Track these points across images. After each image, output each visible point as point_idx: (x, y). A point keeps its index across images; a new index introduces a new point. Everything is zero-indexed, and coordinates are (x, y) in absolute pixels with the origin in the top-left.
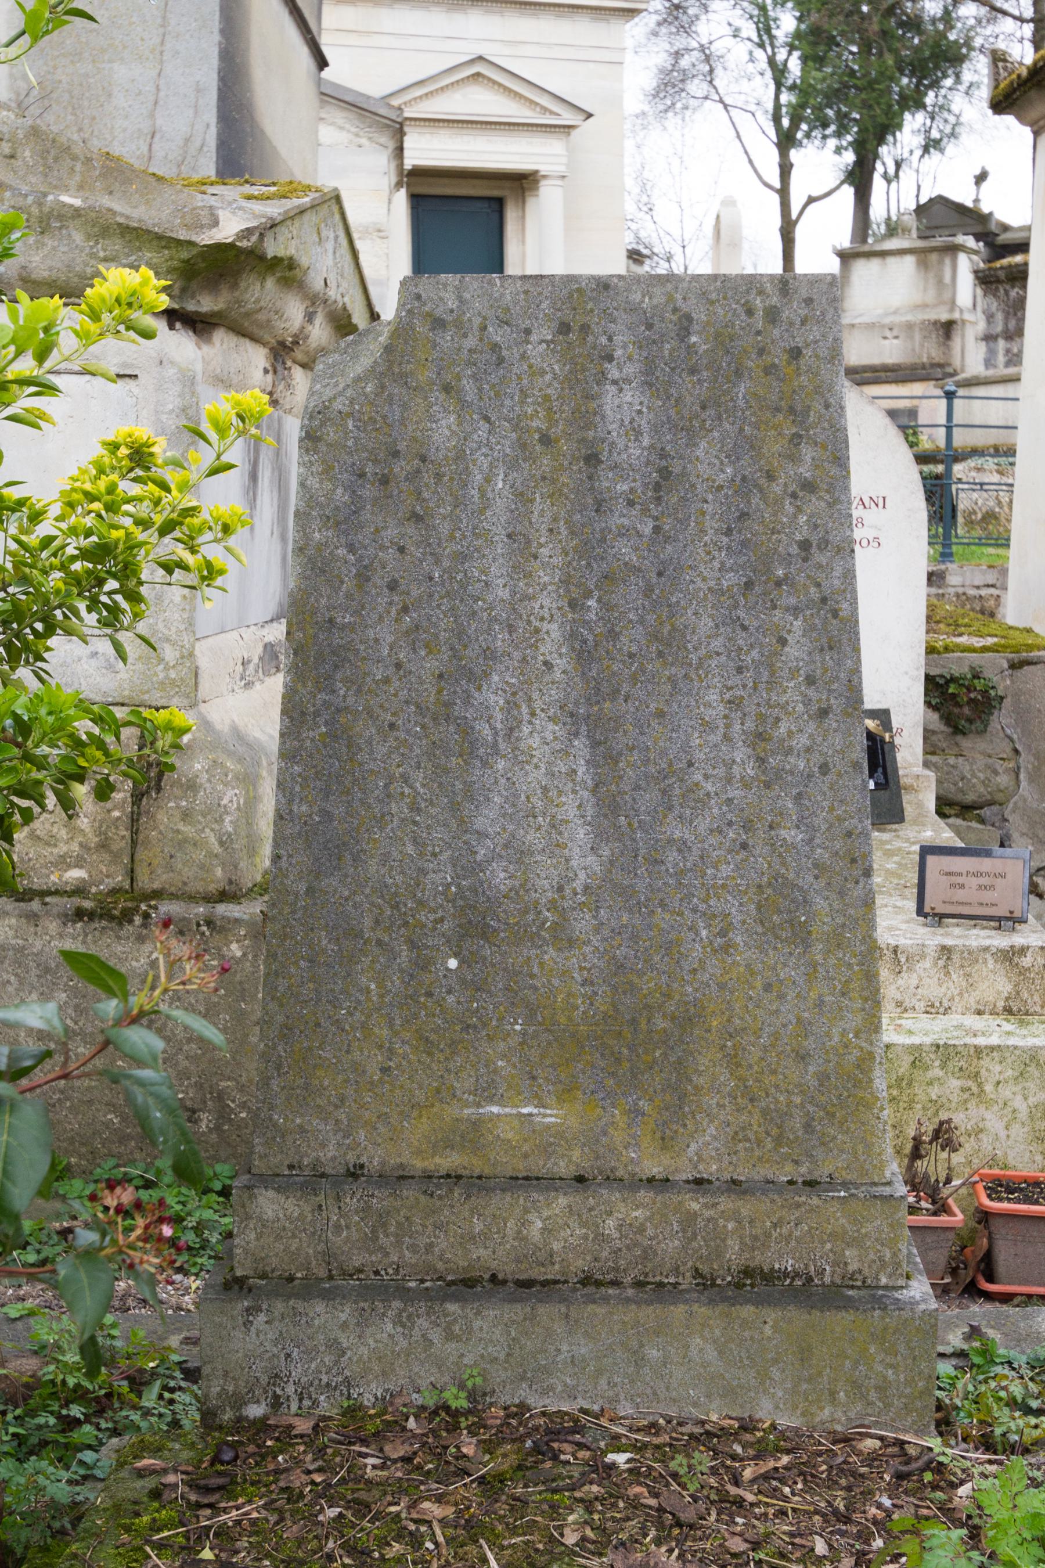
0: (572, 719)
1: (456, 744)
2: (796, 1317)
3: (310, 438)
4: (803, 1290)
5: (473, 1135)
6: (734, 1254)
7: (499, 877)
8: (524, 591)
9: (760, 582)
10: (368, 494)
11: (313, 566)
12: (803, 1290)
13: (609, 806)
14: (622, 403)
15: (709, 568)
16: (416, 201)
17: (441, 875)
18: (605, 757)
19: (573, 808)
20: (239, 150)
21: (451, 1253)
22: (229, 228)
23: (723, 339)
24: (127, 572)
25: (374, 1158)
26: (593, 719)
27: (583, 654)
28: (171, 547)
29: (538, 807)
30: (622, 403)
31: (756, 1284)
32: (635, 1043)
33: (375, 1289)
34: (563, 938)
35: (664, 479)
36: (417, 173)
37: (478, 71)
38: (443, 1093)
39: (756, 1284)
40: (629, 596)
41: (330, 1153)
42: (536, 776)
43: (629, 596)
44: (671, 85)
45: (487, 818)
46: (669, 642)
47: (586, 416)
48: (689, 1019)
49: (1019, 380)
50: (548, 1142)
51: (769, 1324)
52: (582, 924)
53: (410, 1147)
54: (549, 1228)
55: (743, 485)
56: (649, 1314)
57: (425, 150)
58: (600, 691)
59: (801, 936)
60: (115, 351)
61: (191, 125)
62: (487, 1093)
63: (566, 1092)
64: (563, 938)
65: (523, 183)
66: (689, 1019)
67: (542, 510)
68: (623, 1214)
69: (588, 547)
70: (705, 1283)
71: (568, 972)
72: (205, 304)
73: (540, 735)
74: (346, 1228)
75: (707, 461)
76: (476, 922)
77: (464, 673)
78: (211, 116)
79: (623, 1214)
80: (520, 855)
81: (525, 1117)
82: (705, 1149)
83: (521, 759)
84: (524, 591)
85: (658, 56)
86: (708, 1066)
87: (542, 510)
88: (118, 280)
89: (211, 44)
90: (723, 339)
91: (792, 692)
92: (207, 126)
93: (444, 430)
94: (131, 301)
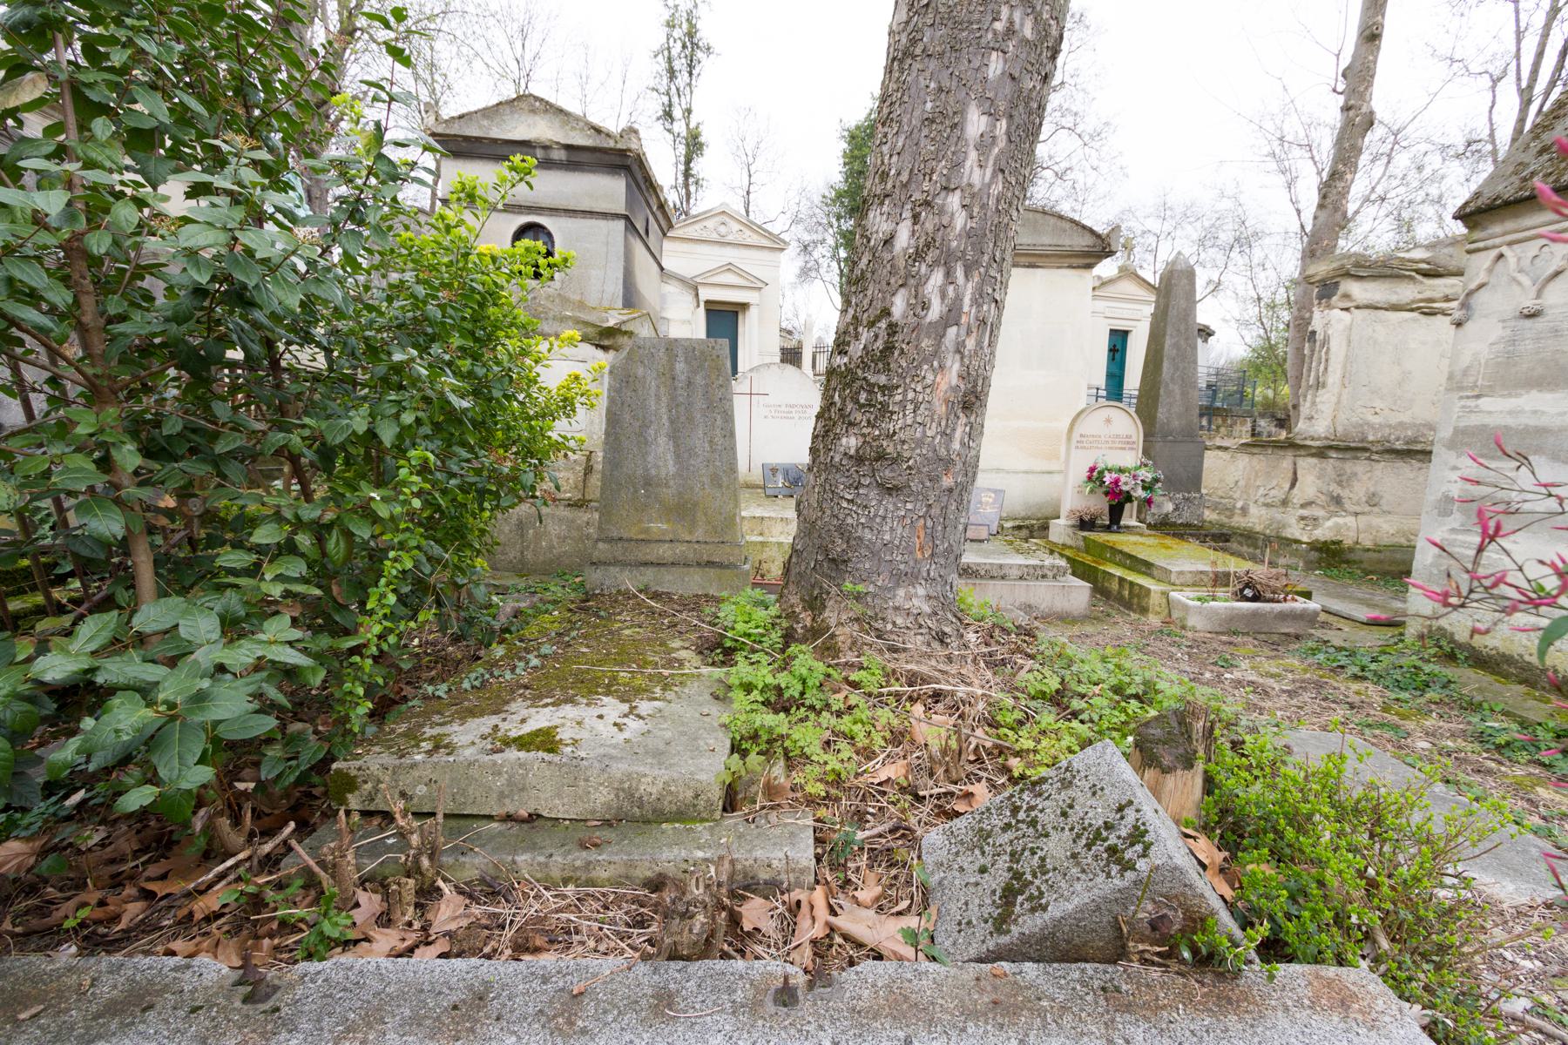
0: (669, 437)
1: (643, 442)
2: (718, 571)
3: (611, 372)
4: (721, 566)
5: (647, 530)
6: (705, 558)
7: (653, 472)
8: (659, 409)
9: (711, 407)
10: (624, 382)
11: (612, 400)
12: (721, 566)
13: (678, 456)
14: (680, 366)
15: (700, 404)
16: (708, 311)
17: (640, 472)
18: (677, 446)
19: (670, 457)
20: (630, 298)
21: (641, 557)
22: (611, 323)
23: (702, 353)
24: (572, 404)
25: (625, 536)
26: (674, 436)
27: (672, 422)
28: (583, 400)
29: (661, 457)
30: (680, 366)
31: (710, 564)
32: (683, 510)
33: (624, 564)
34: (667, 486)
35: (689, 384)
36: (707, 302)
37: (729, 268)
38: (640, 521)
39: (710, 564)
40: (682, 409)
41: (615, 534)
42: (661, 449)
43: (682, 409)
44: (805, 273)
45: (650, 458)
46: (691, 420)
47: (672, 369)
48: (696, 504)
49: (1426, 455)
50: (664, 532)
51: (712, 572)
52: (672, 483)
53: (633, 533)
54: (665, 552)
55: (707, 385)
56: (685, 570)
57: (706, 294)
58: (675, 430)
59: (720, 486)
60: (568, 351)
61: (615, 288)
62: (650, 521)
63: (668, 521)
64: (667, 486)
65: (744, 306)
66: (696, 504)
67: (662, 389)
68: (680, 549)
69: (673, 398)
70: (699, 564)
71: (668, 494)
72: (606, 343)
73: (662, 440)
74: (619, 551)
75: (699, 380)
76: (648, 482)
77: (645, 426)
78: (621, 287)
79: (680, 549)
80: (658, 467)
81: (659, 527)
82: (699, 534)
83: (658, 445)
84: (659, 409)
85: (800, 262)
86: (699, 515)
87: (662, 389)
88: (568, 333)
89: (621, 264)
90: (702, 353)
91: (718, 431)
92: (619, 290)
93: (640, 371)
94: (572, 338)
